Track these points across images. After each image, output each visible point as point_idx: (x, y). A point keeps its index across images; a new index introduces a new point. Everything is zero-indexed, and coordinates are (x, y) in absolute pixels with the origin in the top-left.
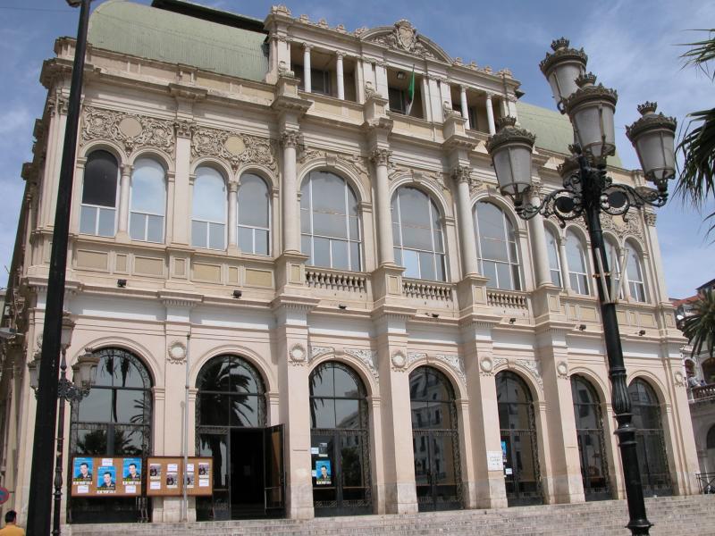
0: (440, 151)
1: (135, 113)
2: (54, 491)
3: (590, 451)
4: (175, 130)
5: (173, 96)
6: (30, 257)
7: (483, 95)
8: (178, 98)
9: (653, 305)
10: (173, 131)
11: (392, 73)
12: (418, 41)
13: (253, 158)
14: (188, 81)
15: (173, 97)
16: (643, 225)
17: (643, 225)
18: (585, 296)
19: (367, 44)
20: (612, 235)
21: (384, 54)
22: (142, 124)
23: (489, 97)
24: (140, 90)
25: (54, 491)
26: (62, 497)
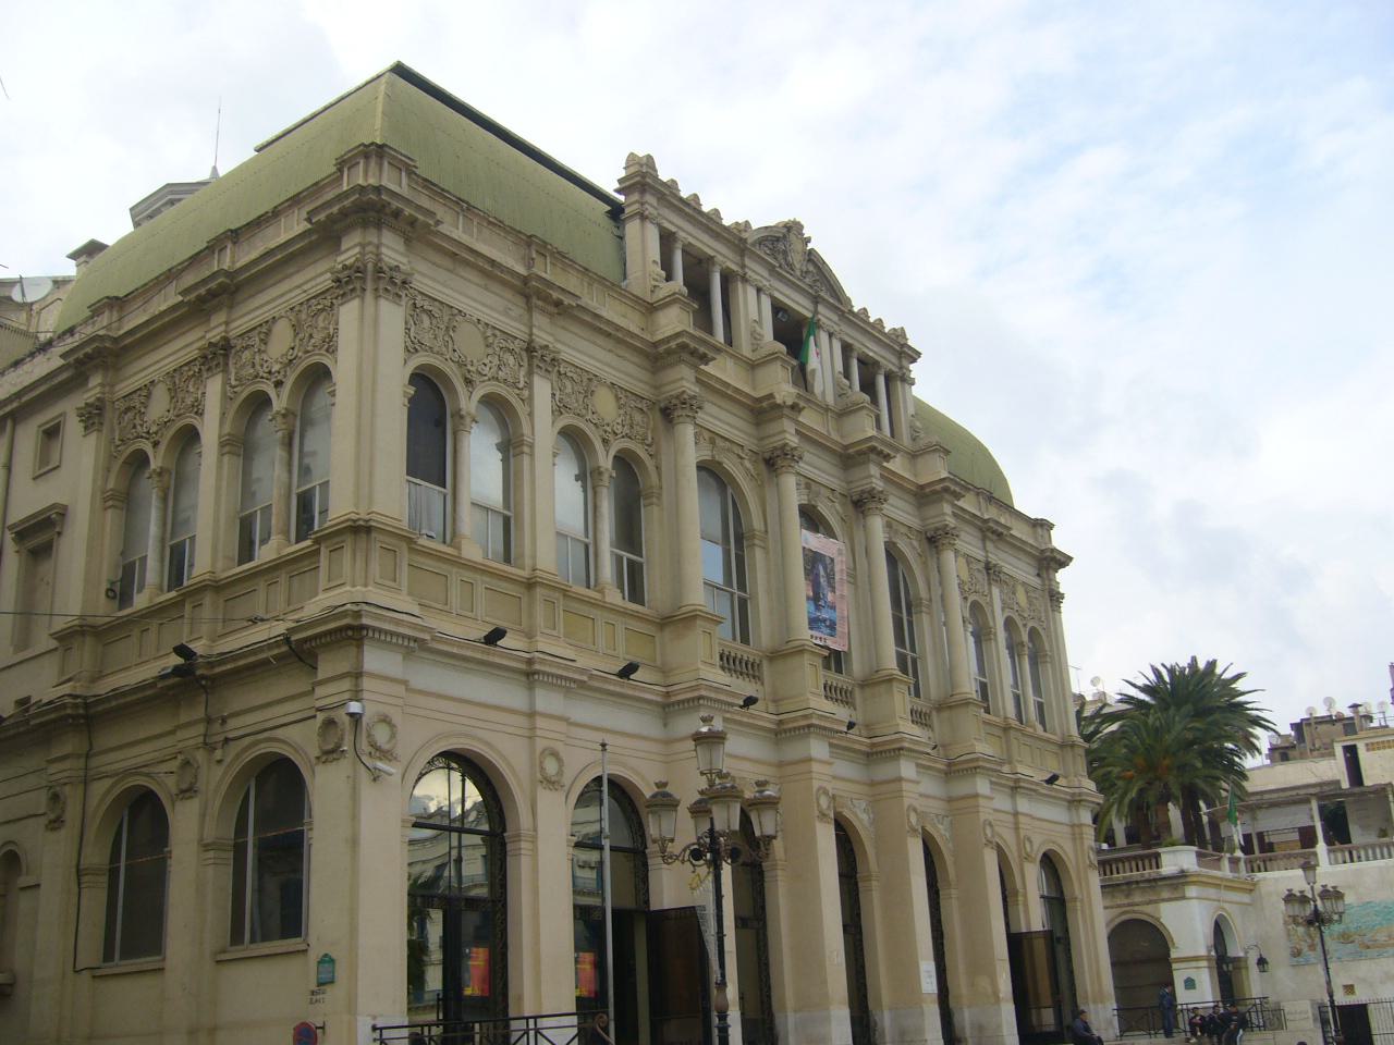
0: (841, 456)
1: (477, 315)
2: (716, 1021)
3: (858, 937)
4: (531, 358)
5: (530, 293)
6: (401, 615)
7: (876, 364)
8: (534, 300)
9: (525, 573)
10: (526, 360)
11: (778, 308)
12: (809, 260)
13: (626, 430)
14: (546, 271)
15: (527, 297)
16: (1046, 606)
17: (1046, 606)
18: (582, 590)
19: (754, 253)
20: (634, 452)
21: (659, 199)
22: (486, 338)
23: (883, 371)
24: (483, 272)
25: (716, 1021)
26: (730, 1031)
